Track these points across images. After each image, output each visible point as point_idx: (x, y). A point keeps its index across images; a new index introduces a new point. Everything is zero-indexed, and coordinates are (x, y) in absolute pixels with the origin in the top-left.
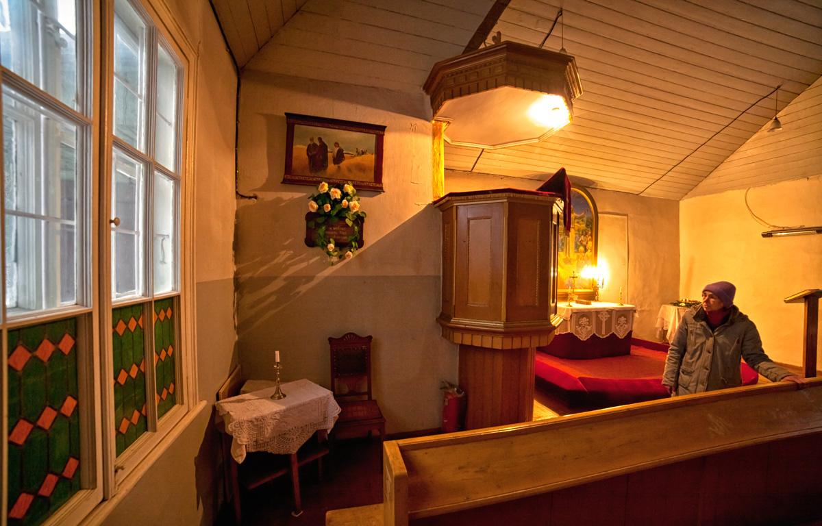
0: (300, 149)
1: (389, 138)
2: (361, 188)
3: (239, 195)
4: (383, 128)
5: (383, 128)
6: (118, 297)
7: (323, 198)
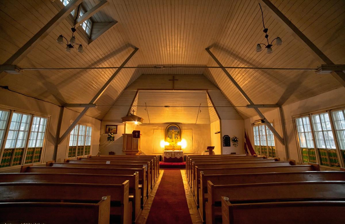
0: (107, 129)
1: (118, 127)
2: (114, 133)
3: (101, 135)
6: (86, 145)
7: (109, 135)
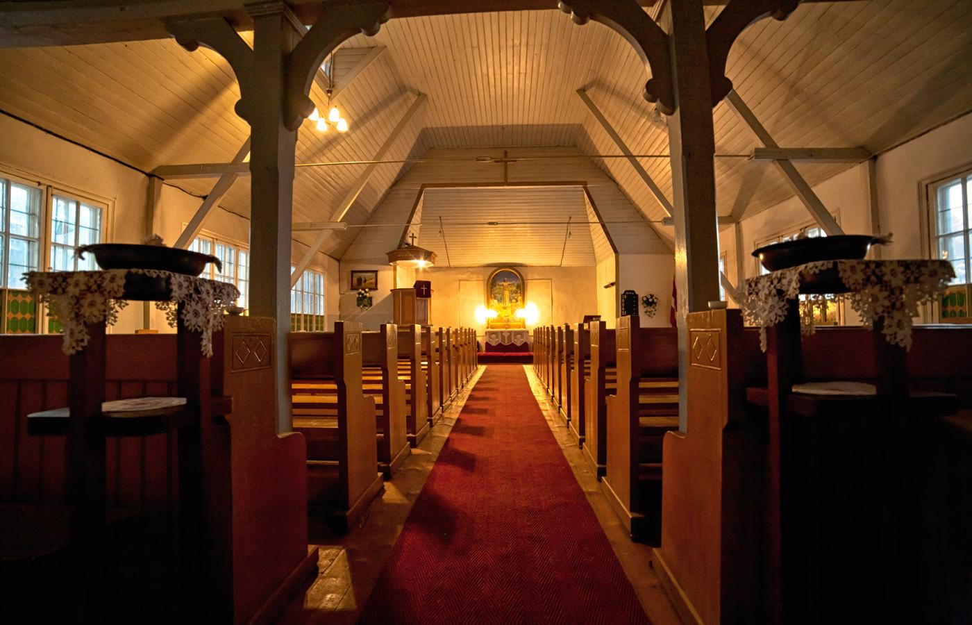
0: (355, 280)
2: (371, 289)
4: (377, 271)
5: (377, 271)
7: (360, 293)
